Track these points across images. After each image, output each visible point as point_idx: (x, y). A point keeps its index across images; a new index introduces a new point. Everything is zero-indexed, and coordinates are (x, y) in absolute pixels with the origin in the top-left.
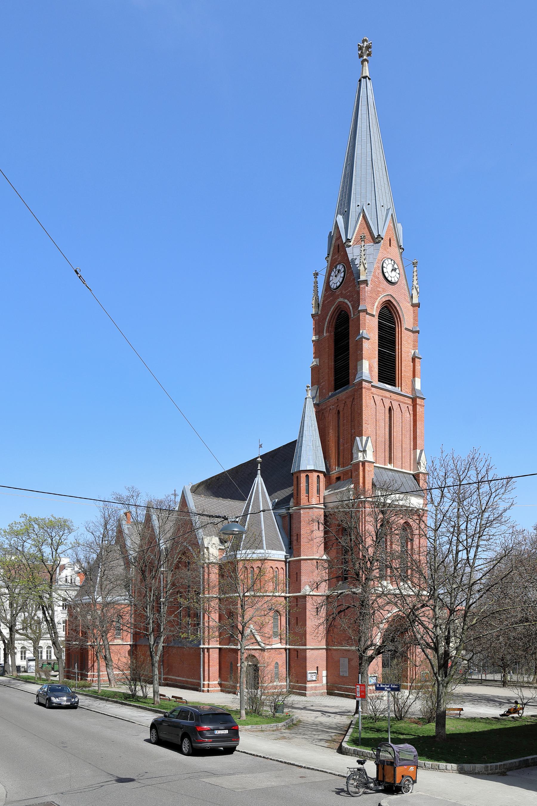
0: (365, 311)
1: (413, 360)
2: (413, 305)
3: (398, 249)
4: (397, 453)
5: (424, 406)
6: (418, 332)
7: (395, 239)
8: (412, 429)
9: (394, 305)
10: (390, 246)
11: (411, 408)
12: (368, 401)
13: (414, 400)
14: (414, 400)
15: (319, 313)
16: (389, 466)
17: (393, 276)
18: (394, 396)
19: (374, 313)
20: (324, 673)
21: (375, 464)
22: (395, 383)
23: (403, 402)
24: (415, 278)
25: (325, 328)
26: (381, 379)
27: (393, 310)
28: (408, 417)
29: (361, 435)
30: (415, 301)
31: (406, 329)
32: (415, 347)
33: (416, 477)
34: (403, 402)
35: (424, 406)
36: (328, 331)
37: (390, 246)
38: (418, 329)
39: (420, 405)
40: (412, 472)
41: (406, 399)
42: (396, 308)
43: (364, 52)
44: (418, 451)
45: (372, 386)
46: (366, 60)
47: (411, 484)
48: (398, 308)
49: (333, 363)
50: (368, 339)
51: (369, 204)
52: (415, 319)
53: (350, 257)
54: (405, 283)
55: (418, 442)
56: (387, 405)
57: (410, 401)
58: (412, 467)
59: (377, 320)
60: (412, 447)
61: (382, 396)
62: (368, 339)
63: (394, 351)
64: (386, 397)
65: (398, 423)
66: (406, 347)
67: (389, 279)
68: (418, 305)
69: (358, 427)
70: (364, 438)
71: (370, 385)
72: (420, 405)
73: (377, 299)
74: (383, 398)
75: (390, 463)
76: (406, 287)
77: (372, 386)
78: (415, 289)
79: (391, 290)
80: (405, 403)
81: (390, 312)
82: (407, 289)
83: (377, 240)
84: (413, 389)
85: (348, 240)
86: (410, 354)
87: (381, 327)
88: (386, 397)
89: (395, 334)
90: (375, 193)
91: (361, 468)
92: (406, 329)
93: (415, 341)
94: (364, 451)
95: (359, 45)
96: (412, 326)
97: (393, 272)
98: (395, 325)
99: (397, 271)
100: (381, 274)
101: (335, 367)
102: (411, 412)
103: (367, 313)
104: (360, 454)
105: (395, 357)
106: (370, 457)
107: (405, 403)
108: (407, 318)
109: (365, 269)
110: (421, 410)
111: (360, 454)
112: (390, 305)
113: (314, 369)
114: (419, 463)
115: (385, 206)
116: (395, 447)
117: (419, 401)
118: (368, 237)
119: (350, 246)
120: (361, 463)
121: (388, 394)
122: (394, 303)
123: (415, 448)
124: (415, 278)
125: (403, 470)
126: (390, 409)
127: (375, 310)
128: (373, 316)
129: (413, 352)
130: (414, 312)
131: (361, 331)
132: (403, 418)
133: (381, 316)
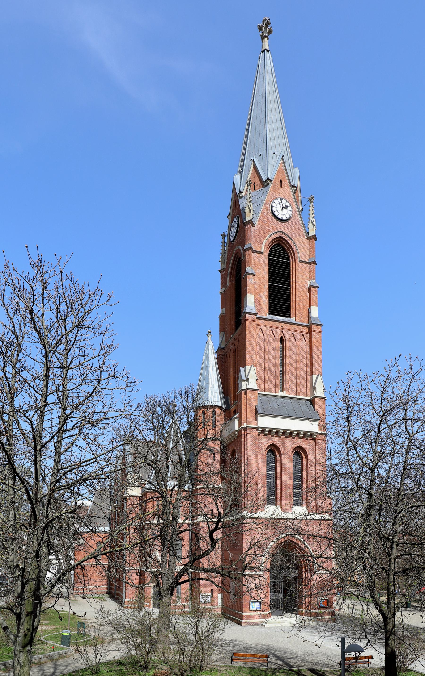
0: (250, 248)
1: (310, 290)
2: (309, 238)
3: (290, 188)
4: (290, 379)
5: (321, 332)
6: (314, 262)
7: (287, 180)
8: (308, 355)
9: (286, 241)
10: (281, 187)
11: (307, 336)
12: (252, 332)
13: (310, 328)
14: (310, 328)
15: (225, 267)
16: (280, 394)
17: (284, 214)
18: (285, 326)
19: (262, 250)
20: (220, 596)
21: (259, 392)
22: (290, 315)
23: (297, 331)
24: (312, 212)
25: (228, 279)
26: (271, 312)
27: (286, 246)
28: (304, 345)
29: (244, 366)
30: (311, 234)
31: (301, 262)
32: (311, 277)
33: (312, 402)
34: (297, 331)
35: (321, 332)
36: (230, 281)
37: (281, 187)
38: (314, 259)
39: (315, 331)
40: (309, 398)
41: (301, 327)
42: (288, 243)
43: (265, 29)
44: (314, 377)
45: (258, 318)
46: (266, 37)
47: (306, 407)
48: (291, 243)
49: (234, 308)
50: (254, 275)
51: (260, 155)
52: (312, 251)
53: (241, 206)
54: (300, 218)
55: (314, 368)
56: (278, 335)
57: (306, 330)
58: (309, 393)
59: (268, 257)
60: (308, 373)
61: (272, 327)
62: (254, 275)
63: (289, 284)
64: (276, 328)
65: (291, 352)
66: (301, 279)
67: (280, 217)
68: (314, 237)
69: (243, 358)
70: (248, 368)
71: (255, 316)
72: (315, 331)
73: (265, 237)
74: (273, 329)
75: (283, 391)
76: (300, 222)
77: (258, 318)
78: (311, 224)
79: (282, 227)
80: (299, 332)
81: (283, 248)
82: (301, 224)
83: (265, 184)
84: (310, 317)
85: (241, 192)
86: (306, 284)
87: (271, 263)
88: (276, 328)
89: (290, 269)
90: (274, 149)
91: (244, 396)
92: (301, 262)
93: (312, 272)
94: (247, 380)
95: (258, 26)
96: (308, 258)
97: (284, 210)
98: (289, 260)
99: (289, 208)
100: (271, 214)
101: (236, 311)
102: (308, 340)
103: (254, 251)
104: (243, 384)
105: (290, 291)
106: (253, 384)
107: (299, 332)
108: (301, 250)
109: (250, 210)
110: (318, 336)
111: (243, 384)
112: (282, 242)
113: (222, 318)
114: (315, 388)
115: (278, 153)
116: (287, 375)
117: (314, 328)
118: (258, 183)
119: (242, 197)
120: (243, 392)
121: (278, 325)
122: (286, 238)
123: (311, 374)
124: (312, 212)
125: (298, 397)
126: (282, 340)
127: (264, 247)
128: (261, 253)
129: (309, 282)
130: (310, 245)
131: (246, 269)
132: (297, 345)
133: (271, 253)
